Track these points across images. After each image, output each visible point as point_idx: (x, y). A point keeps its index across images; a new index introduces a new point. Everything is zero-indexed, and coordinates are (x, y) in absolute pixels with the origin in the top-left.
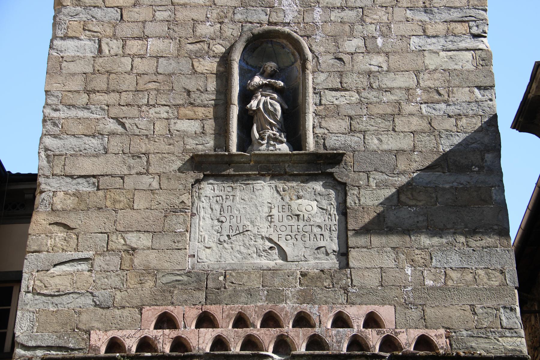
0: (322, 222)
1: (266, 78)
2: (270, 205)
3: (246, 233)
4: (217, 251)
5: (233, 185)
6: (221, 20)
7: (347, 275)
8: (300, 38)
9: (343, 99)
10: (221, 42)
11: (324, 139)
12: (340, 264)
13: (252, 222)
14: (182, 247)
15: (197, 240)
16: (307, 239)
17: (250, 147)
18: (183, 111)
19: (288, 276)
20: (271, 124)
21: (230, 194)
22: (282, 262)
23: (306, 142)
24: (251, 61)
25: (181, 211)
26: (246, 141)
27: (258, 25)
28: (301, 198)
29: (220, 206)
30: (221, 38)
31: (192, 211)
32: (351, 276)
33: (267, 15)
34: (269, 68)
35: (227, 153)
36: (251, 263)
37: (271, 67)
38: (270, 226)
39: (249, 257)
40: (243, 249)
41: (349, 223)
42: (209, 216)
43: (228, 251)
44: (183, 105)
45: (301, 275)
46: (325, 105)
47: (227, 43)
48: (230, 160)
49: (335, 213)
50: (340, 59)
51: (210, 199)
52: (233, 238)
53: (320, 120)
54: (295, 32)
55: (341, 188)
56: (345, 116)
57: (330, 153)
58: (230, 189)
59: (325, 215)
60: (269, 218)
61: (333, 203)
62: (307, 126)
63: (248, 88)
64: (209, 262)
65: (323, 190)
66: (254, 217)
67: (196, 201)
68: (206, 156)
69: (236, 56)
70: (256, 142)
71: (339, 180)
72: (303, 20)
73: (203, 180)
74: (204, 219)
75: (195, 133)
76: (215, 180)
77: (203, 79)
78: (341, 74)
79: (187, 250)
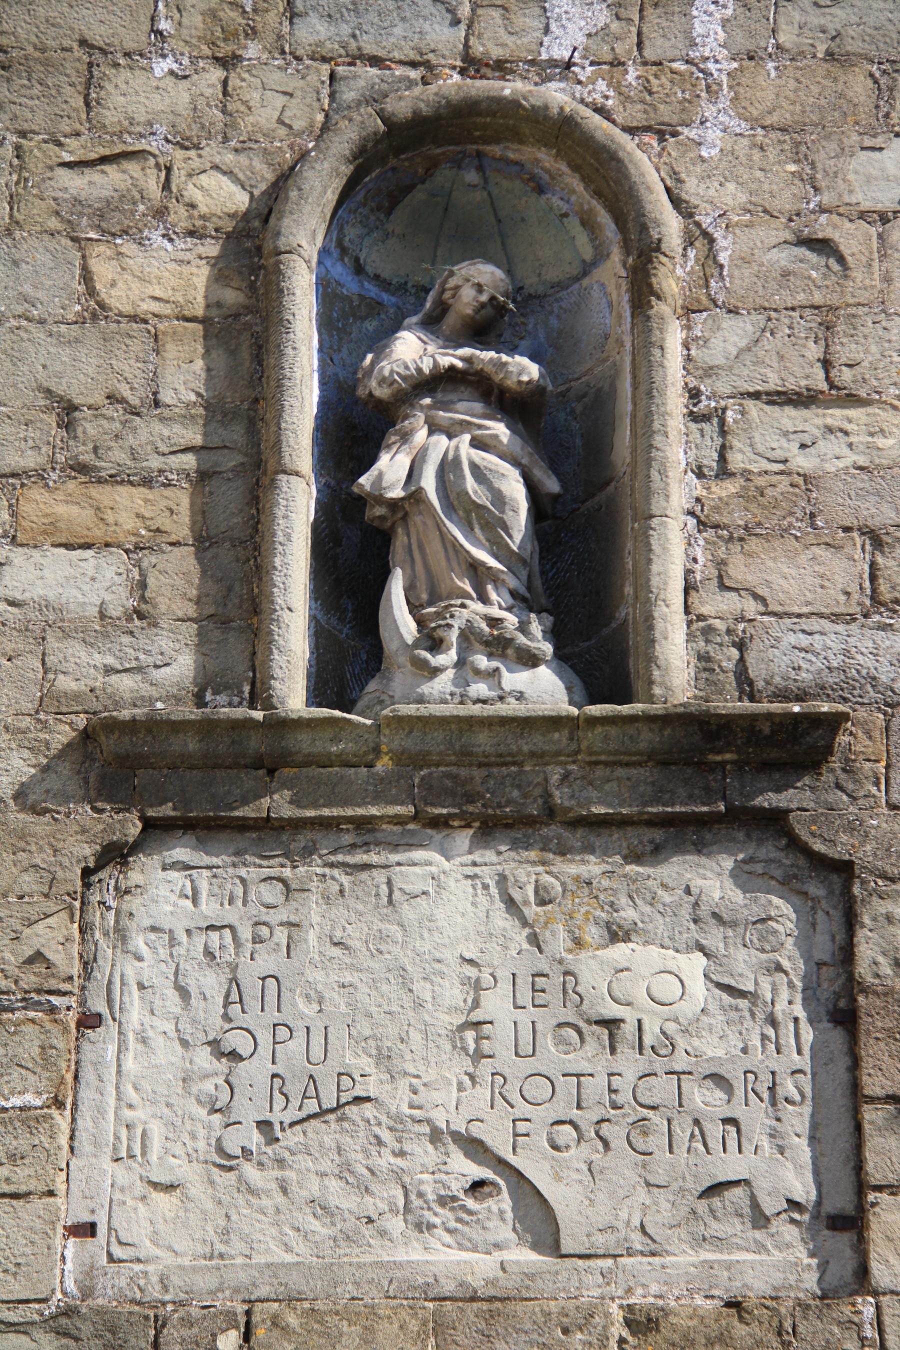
0: (732, 1059)
1: (453, 341)
2: (472, 972)
3: (352, 1111)
4: (209, 1205)
5: (287, 872)
6: (225, 49)
7: (859, 1326)
8: (624, 139)
9: (833, 446)
10: (229, 158)
11: (741, 646)
12: (823, 1268)
13: (383, 1058)
14: (32, 1185)
15: (109, 1150)
16: (657, 1142)
17: (372, 686)
18: (38, 503)
19: (566, 1331)
20: (477, 572)
21: (274, 917)
22: (533, 1256)
23: (651, 660)
24: (376, 259)
25: (28, 1004)
26: (350, 654)
27: (414, 74)
28: (627, 939)
29: (224, 978)
30: (226, 139)
31: (82, 1003)
32: (881, 1331)
33: (456, 22)
34: (468, 294)
35: (258, 715)
36: (380, 1265)
37: (479, 288)
38: (472, 1077)
39: (367, 1231)
40: (337, 1194)
41: (867, 1065)
42: (170, 1027)
43: (266, 1202)
44: (40, 475)
45: (628, 1323)
46: (746, 474)
47: (258, 165)
48: (270, 751)
49: (799, 1010)
50: (823, 246)
51: (173, 942)
52: (292, 1138)
53: (721, 553)
54: (600, 110)
55: (831, 884)
56: (847, 529)
57: (769, 716)
58: (272, 893)
59: (748, 1023)
60: (470, 1035)
61: (786, 964)
62: (655, 581)
63: (361, 392)
64: (168, 1259)
65: (738, 897)
66: (392, 1030)
67: (106, 950)
68: (153, 726)
69: (305, 233)
70: (403, 659)
71: (818, 846)
72: (640, 45)
73: (136, 847)
74: (144, 1041)
75: (102, 615)
76: (202, 845)
77: (136, 346)
78: (827, 320)
79: (60, 1201)
